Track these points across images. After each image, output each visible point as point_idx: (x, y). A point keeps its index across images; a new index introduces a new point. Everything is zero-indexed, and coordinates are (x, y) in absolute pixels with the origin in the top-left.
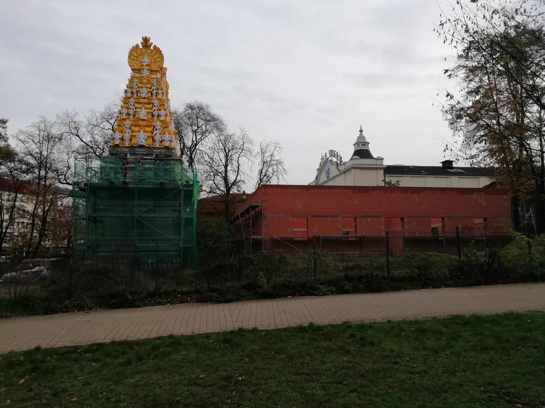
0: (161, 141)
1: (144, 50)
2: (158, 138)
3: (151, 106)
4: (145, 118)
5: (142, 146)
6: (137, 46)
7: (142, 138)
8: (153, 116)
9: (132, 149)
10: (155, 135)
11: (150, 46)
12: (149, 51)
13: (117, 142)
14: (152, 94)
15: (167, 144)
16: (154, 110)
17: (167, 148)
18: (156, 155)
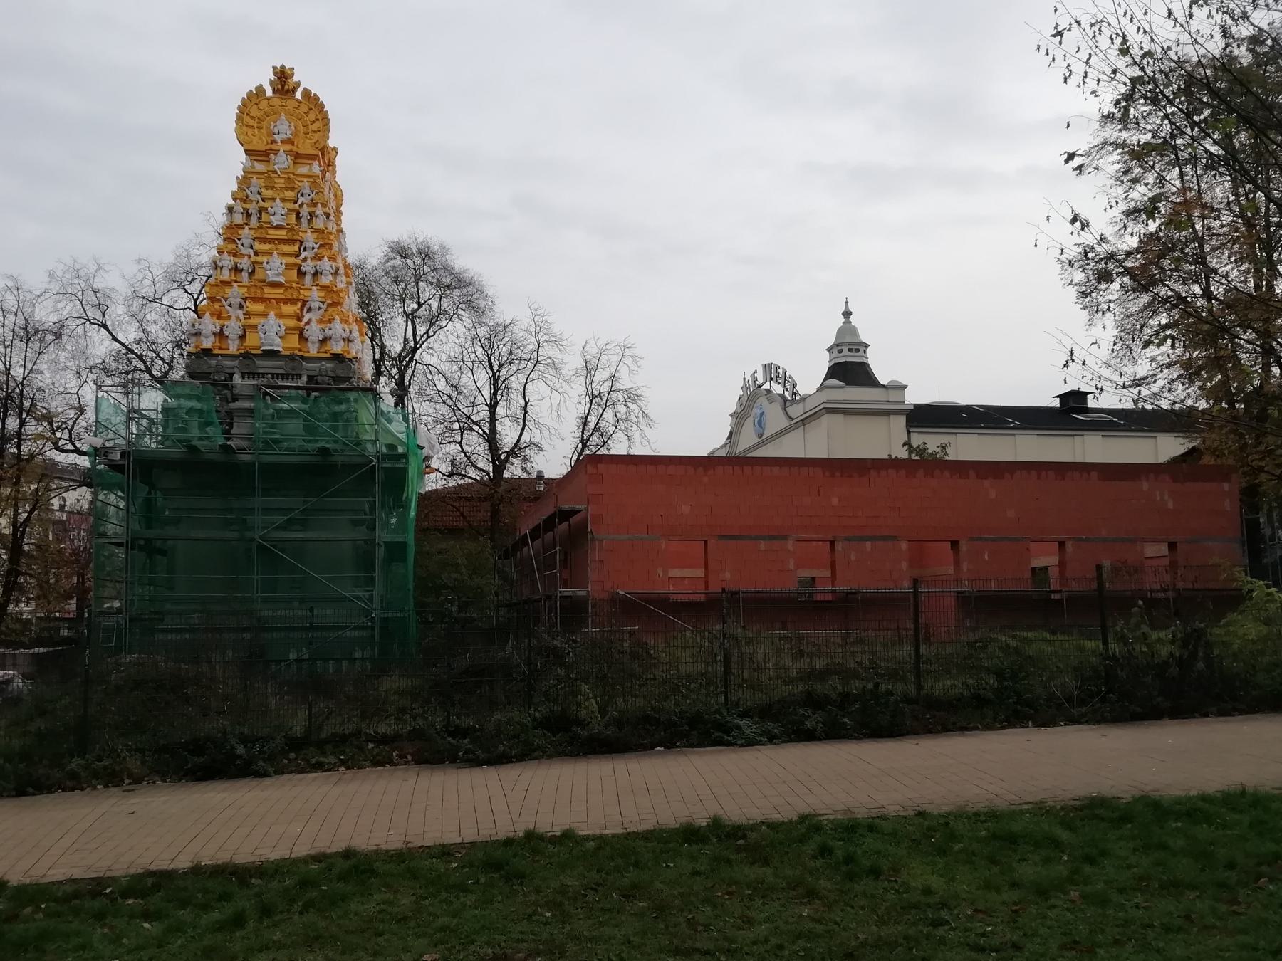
0: (324, 341)
1: (277, 102)
2: (314, 331)
3: (296, 248)
4: (282, 279)
5: (272, 354)
6: (260, 89)
7: (272, 332)
8: (301, 274)
9: (247, 362)
10: (308, 323)
11: (294, 91)
12: (290, 104)
13: (207, 343)
14: (298, 217)
15: (338, 348)
16: (305, 260)
17: (338, 358)
18: (310, 378)
